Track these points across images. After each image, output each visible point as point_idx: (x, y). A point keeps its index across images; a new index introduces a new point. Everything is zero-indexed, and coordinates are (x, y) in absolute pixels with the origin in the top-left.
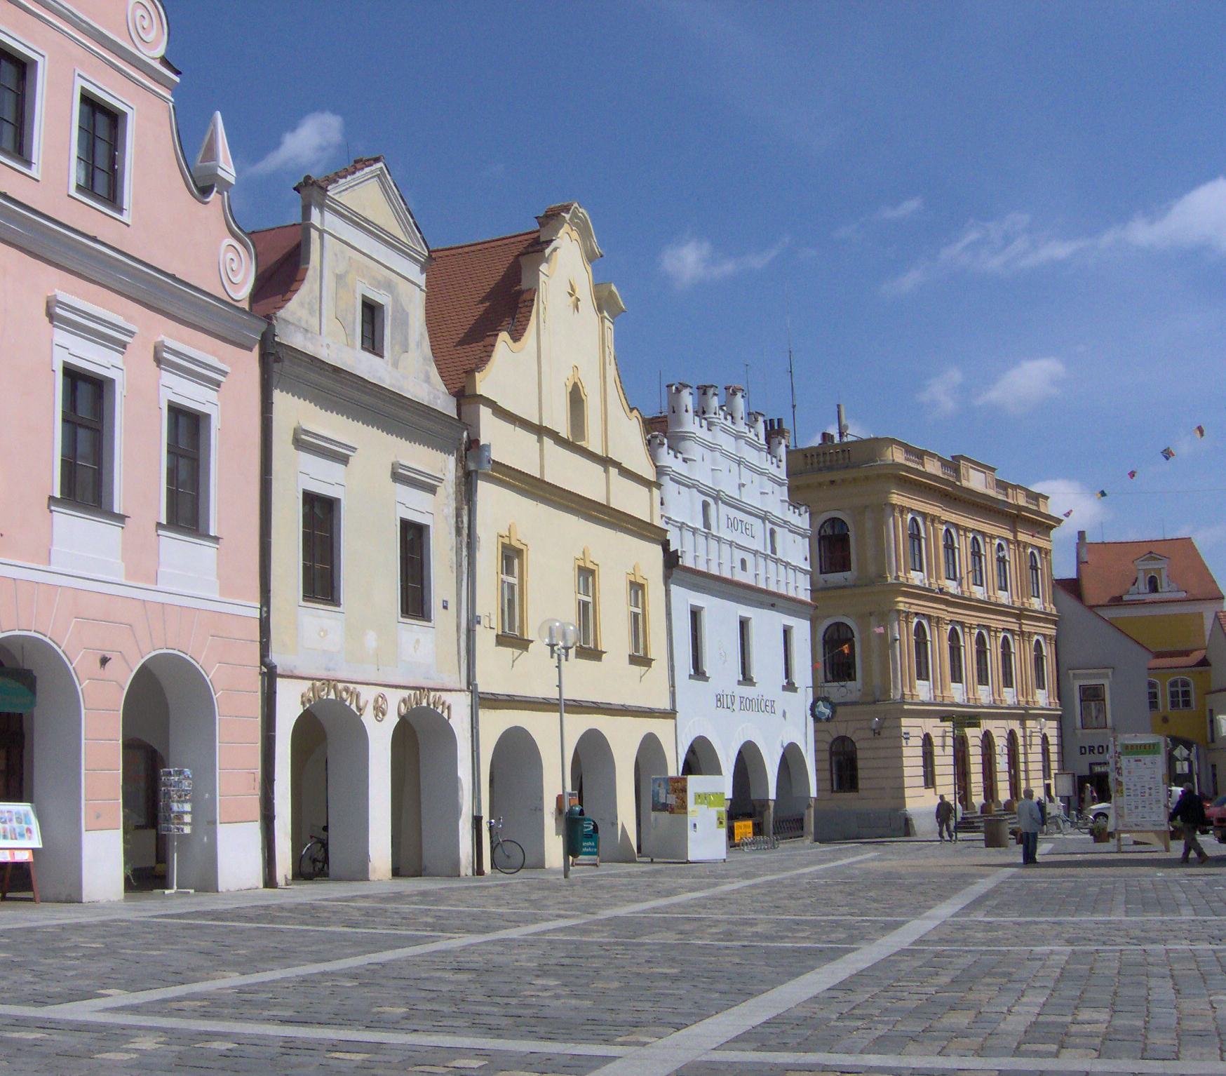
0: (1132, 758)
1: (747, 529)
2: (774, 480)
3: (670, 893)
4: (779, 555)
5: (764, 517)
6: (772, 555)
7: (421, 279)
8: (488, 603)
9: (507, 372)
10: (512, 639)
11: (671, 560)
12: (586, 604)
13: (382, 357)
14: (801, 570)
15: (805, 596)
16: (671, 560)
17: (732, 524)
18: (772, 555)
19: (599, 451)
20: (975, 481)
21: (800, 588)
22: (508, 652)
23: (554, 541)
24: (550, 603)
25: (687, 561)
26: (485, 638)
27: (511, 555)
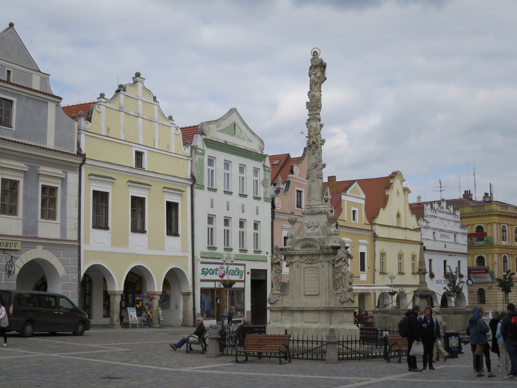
0: (425, 230)
1: (447, 237)
2: (456, 222)
3: (430, 379)
4: (457, 242)
5: (450, 232)
6: (456, 243)
7: (363, 196)
8: (378, 266)
9: (385, 216)
10: (383, 273)
12: (401, 263)
13: (107, 228)
14: (465, 245)
15: (466, 252)
17: (442, 236)
18: (456, 243)
19: (404, 227)
21: (465, 250)
22: (382, 276)
23: (392, 251)
24: (392, 266)
25: (427, 248)
26: (377, 274)
27: (383, 255)
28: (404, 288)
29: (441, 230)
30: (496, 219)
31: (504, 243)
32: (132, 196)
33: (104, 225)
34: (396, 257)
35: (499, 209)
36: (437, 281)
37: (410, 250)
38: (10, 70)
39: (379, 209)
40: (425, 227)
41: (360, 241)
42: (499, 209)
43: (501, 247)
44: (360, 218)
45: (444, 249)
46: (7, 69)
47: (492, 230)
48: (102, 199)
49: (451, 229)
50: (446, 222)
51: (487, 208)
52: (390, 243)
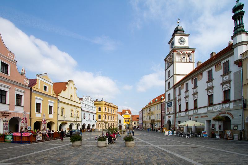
11: (82, 110)
16: (82, 110)
17: (88, 107)
20: (112, 105)
28: (73, 122)
29: (88, 105)
30: (104, 105)
31: (106, 112)
32: (49, 106)
33: (4, 102)
34: (70, 111)
35: (105, 103)
36: (86, 121)
37: (112, 123)
38: (46, 86)
39: (62, 90)
40: (82, 103)
41: (36, 97)
42: (105, 103)
43: (105, 113)
44: (49, 90)
45: (89, 111)
46: (44, 85)
47: (103, 108)
48: (113, 125)
49: (92, 105)
50: (90, 103)
51: (102, 102)
52: (64, 104)
